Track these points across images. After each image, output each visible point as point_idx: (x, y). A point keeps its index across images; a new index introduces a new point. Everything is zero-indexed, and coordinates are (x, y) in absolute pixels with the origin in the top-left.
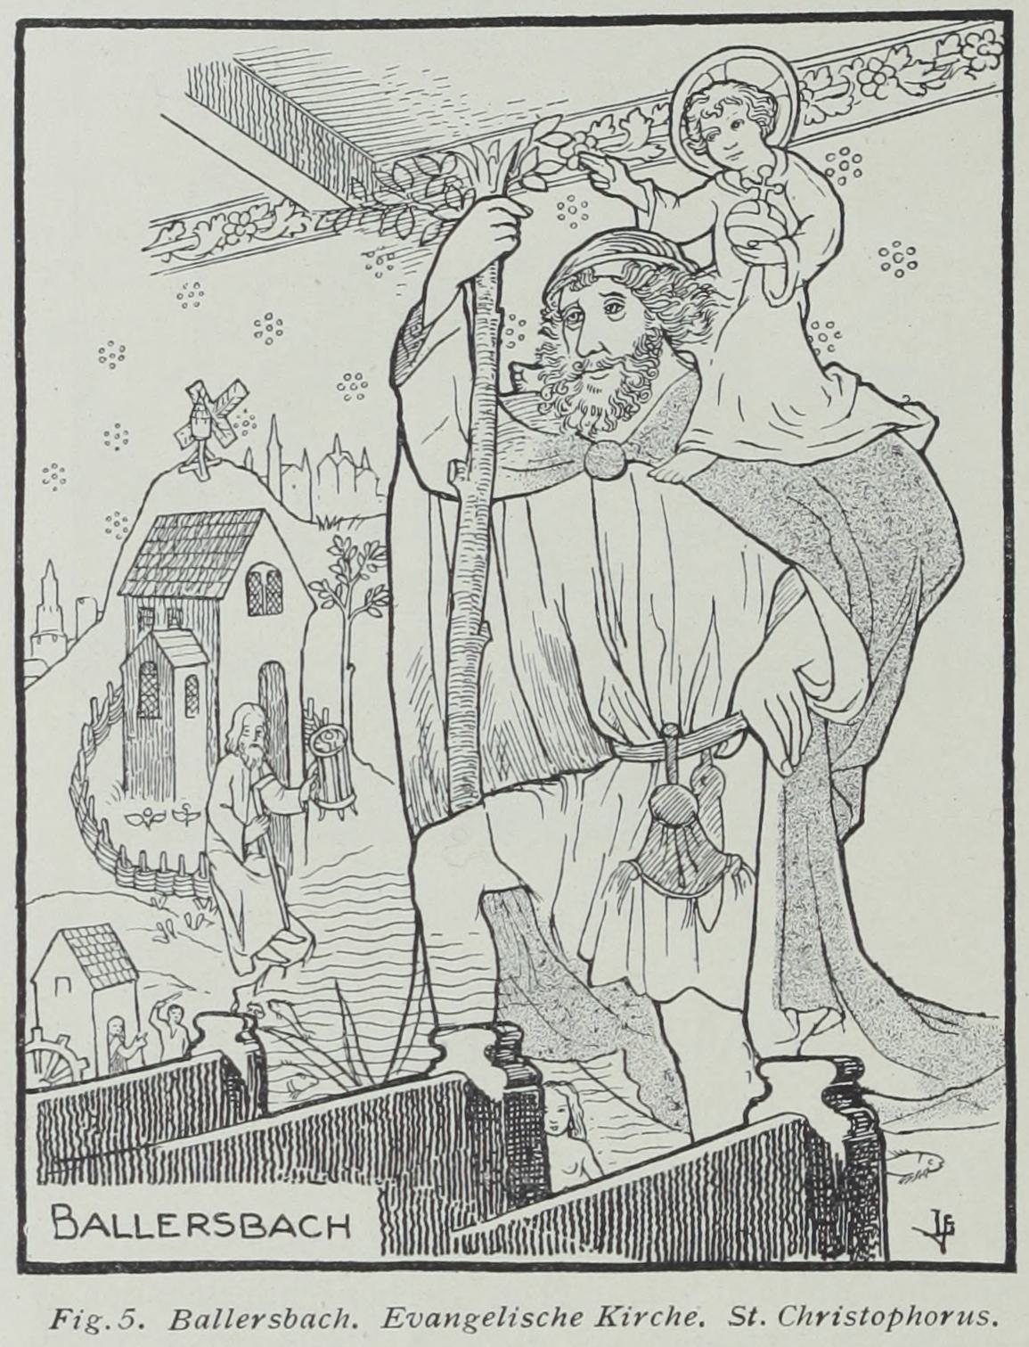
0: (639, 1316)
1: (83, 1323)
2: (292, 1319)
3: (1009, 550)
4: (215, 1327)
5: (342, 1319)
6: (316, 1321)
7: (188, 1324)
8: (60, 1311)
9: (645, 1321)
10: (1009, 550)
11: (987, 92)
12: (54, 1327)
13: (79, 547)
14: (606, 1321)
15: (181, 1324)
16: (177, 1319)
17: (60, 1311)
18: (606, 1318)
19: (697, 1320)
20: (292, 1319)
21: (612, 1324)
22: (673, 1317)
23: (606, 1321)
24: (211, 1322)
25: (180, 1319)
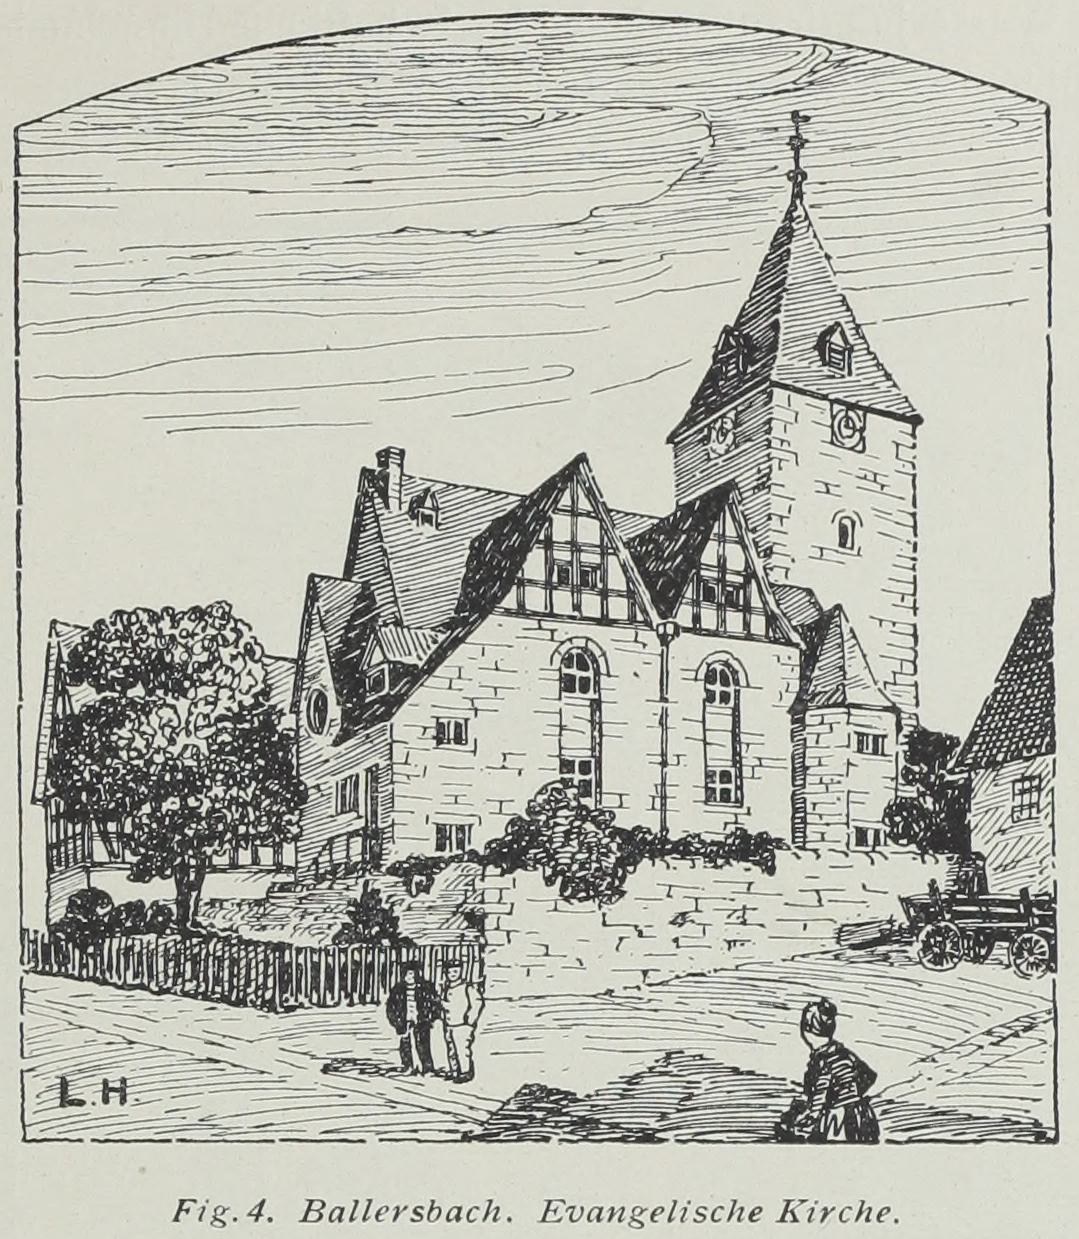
1: (208, 1215)
7: (321, 1216)
9: (833, 1216)
12: (176, 1219)
14: (789, 1217)
16: (309, 1209)
17: (182, 1202)
20: (436, 1212)
21: (795, 1220)
23: (789, 1217)
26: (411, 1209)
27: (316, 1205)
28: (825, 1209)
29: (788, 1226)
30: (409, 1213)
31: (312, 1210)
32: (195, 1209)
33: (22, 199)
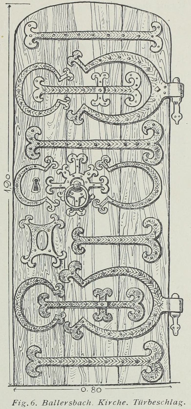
0: (110, 402)
1: (21, 404)
2: (75, 403)
3: (169, 273)
4: (171, 404)
5: (89, 403)
6: (82, 403)
7: (47, 404)
8: (15, 401)
9: (112, 404)
10: (169, 273)
11: (93, 250)
12: (13, 405)
13: (184, 318)
14: (101, 404)
15: (45, 404)
16: (44, 402)
17: (15, 401)
18: (101, 403)
19: (126, 404)
20: (75, 403)
21: (102, 404)
22: (119, 403)
23: (101, 404)
24: (53, 404)
25: (45, 402)
26: (69, 402)
27: (46, 401)
28: (110, 402)
29: (101, 406)
30: (68, 403)
31: (45, 402)
32: (18, 402)
33: (93, 4)
